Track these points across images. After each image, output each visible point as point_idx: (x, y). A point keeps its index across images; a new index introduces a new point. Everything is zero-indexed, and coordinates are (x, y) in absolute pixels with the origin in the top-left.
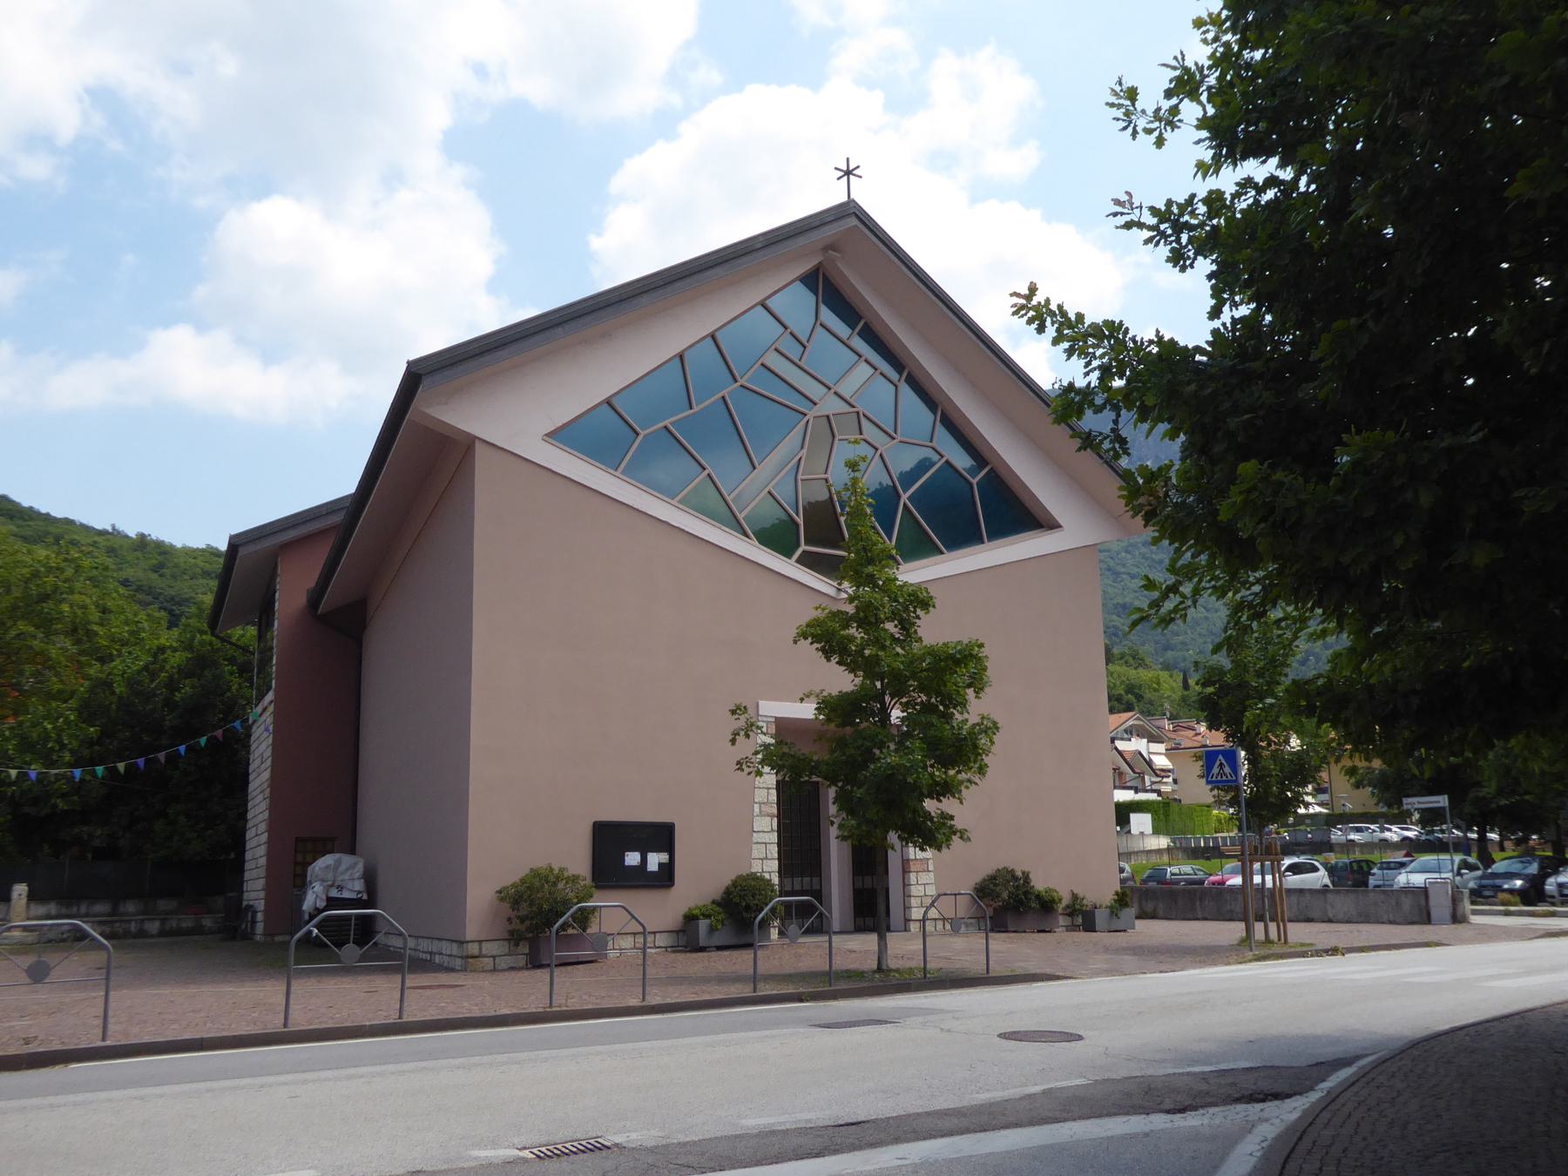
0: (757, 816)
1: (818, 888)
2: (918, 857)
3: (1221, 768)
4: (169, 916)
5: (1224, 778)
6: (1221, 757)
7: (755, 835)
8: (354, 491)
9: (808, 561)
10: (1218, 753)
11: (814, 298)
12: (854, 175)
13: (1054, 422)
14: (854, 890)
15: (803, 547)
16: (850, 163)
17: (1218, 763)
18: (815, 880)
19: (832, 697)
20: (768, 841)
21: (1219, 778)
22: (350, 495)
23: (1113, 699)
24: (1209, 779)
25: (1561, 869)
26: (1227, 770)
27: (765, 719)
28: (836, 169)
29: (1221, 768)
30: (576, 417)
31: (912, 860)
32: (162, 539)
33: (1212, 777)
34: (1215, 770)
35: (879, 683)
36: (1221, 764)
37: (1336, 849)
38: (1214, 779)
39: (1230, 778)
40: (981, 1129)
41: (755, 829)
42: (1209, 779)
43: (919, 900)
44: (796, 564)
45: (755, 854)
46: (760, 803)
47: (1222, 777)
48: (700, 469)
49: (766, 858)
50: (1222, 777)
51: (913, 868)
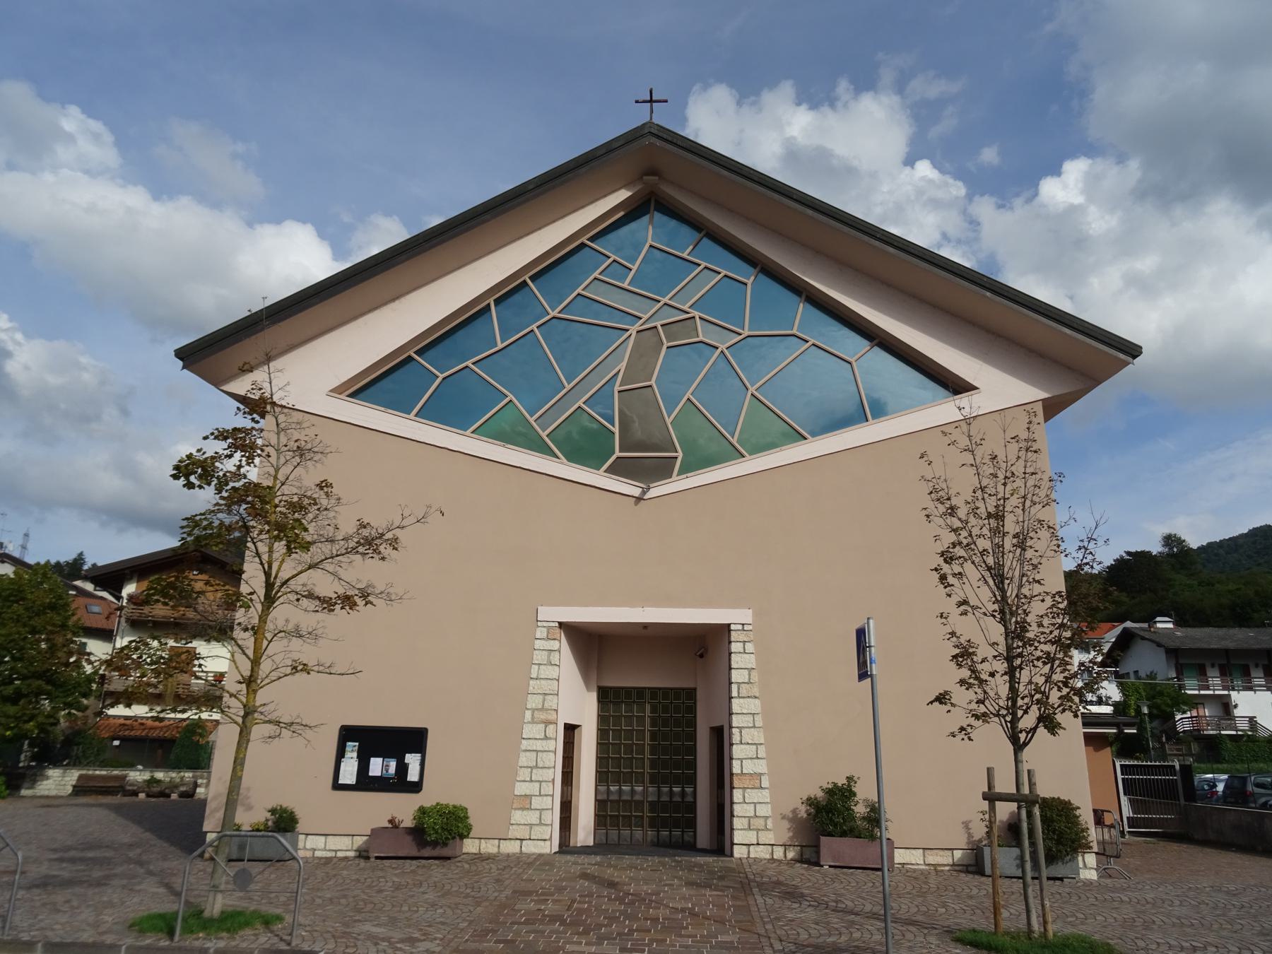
0: (529, 723)
1: (692, 800)
2: (745, 771)
4: (249, 833)
7: (523, 741)
9: (618, 469)
11: (587, 249)
13: (49, 561)
14: (596, 800)
15: (617, 454)
18: (689, 790)
20: (538, 749)
22: (192, 371)
25: (140, 767)
27: (545, 624)
30: (497, 285)
31: (737, 774)
41: (524, 736)
43: (745, 821)
44: (875, 421)
45: (524, 759)
46: (533, 710)
48: (693, 320)
49: (537, 767)
51: (736, 784)
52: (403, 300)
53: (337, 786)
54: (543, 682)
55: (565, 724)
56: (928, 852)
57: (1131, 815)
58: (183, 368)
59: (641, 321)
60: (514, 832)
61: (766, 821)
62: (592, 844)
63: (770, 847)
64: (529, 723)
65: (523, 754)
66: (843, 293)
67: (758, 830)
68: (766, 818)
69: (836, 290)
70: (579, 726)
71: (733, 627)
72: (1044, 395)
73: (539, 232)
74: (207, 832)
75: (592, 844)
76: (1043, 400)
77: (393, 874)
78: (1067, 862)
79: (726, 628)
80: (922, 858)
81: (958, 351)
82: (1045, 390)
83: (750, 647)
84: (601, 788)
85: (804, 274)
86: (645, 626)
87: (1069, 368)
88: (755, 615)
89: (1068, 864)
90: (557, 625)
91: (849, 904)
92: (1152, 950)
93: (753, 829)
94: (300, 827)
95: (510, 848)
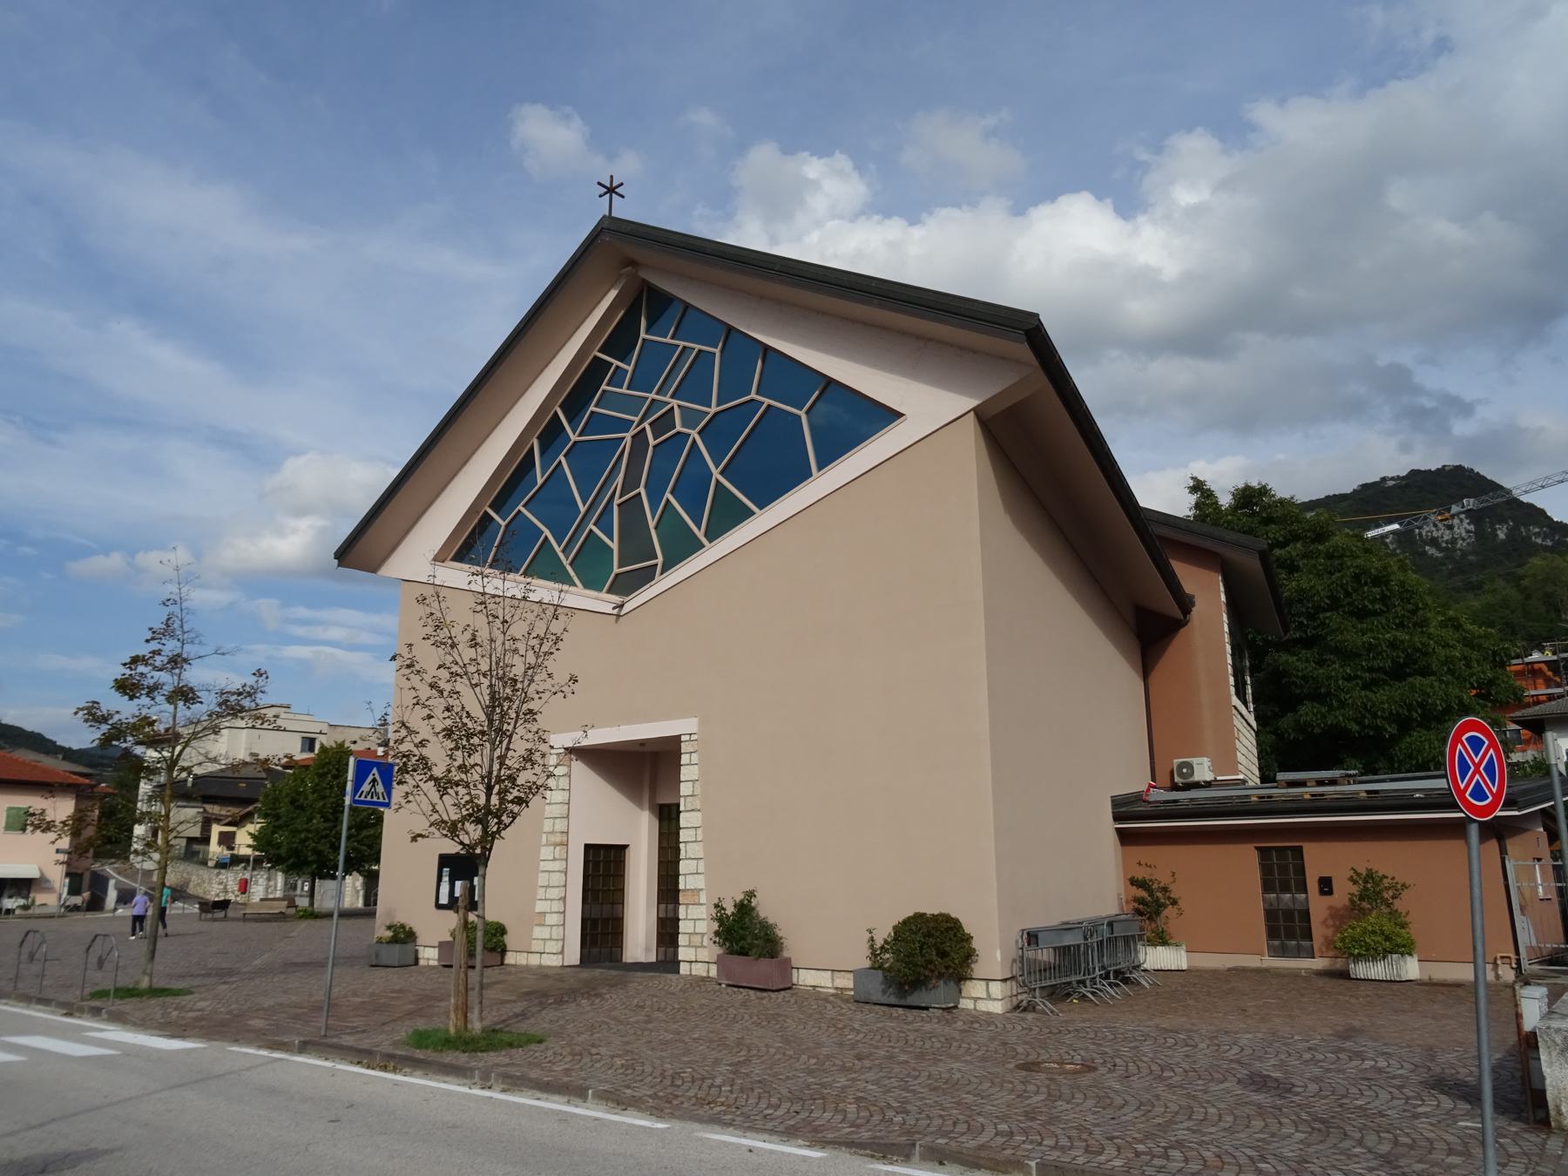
0: (544, 845)
3: (373, 786)
5: (375, 799)
6: (375, 771)
8: (1555, 520)
10: (372, 765)
12: (617, 193)
16: (618, 197)
17: (370, 778)
19: (972, 962)
21: (369, 798)
23: (470, 963)
24: (357, 798)
26: (380, 788)
28: (623, 197)
29: (373, 786)
32: (780, 934)
33: (360, 797)
34: (366, 787)
35: (492, 803)
36: (374, 780)
37: (1283, 783)
38: (362, 798)
39: (381, 800)
40: (504, 542)
42: (357, 798)
47: (372, 797)
50: (372, 797)
52: (471, 461)
53: (439, 906)
54: (554, 806)
55: (587, 847)
56: (836, 974)
57: (1534, 943)
58: (339, 566)
59: (635, 425)
60: (537, 946)
61: (702, 938)
62: (654, 960)
63: (706, 964)
64: (544, 845)
65: (540, 875)
66: (779, 337)
67: (696, 947)
68: (703, 934)
69: (785, 340)
70: (628, 846)
71: (683, 738)
72: (973, 403)
73: (554, 360)
74: (680, 961)
75: (654, 960)
76: (976, 410)
77: (872, 1015)
78: (931, 990)
79: (676, 740)
80: (830, 981)
81: (887, 375)
82: (971, 395)
83: (695, 758)
84: (663, 906)
85: (749, 327)
86: (642, 743)
87: (1003, 358)
88: (701, 724)
89: (932, 991)
90: (563, 750)
91: (322, 993)
92: (618, 1056)
93: (693, 947)
94: (419, 941)
95: (534, 960)
